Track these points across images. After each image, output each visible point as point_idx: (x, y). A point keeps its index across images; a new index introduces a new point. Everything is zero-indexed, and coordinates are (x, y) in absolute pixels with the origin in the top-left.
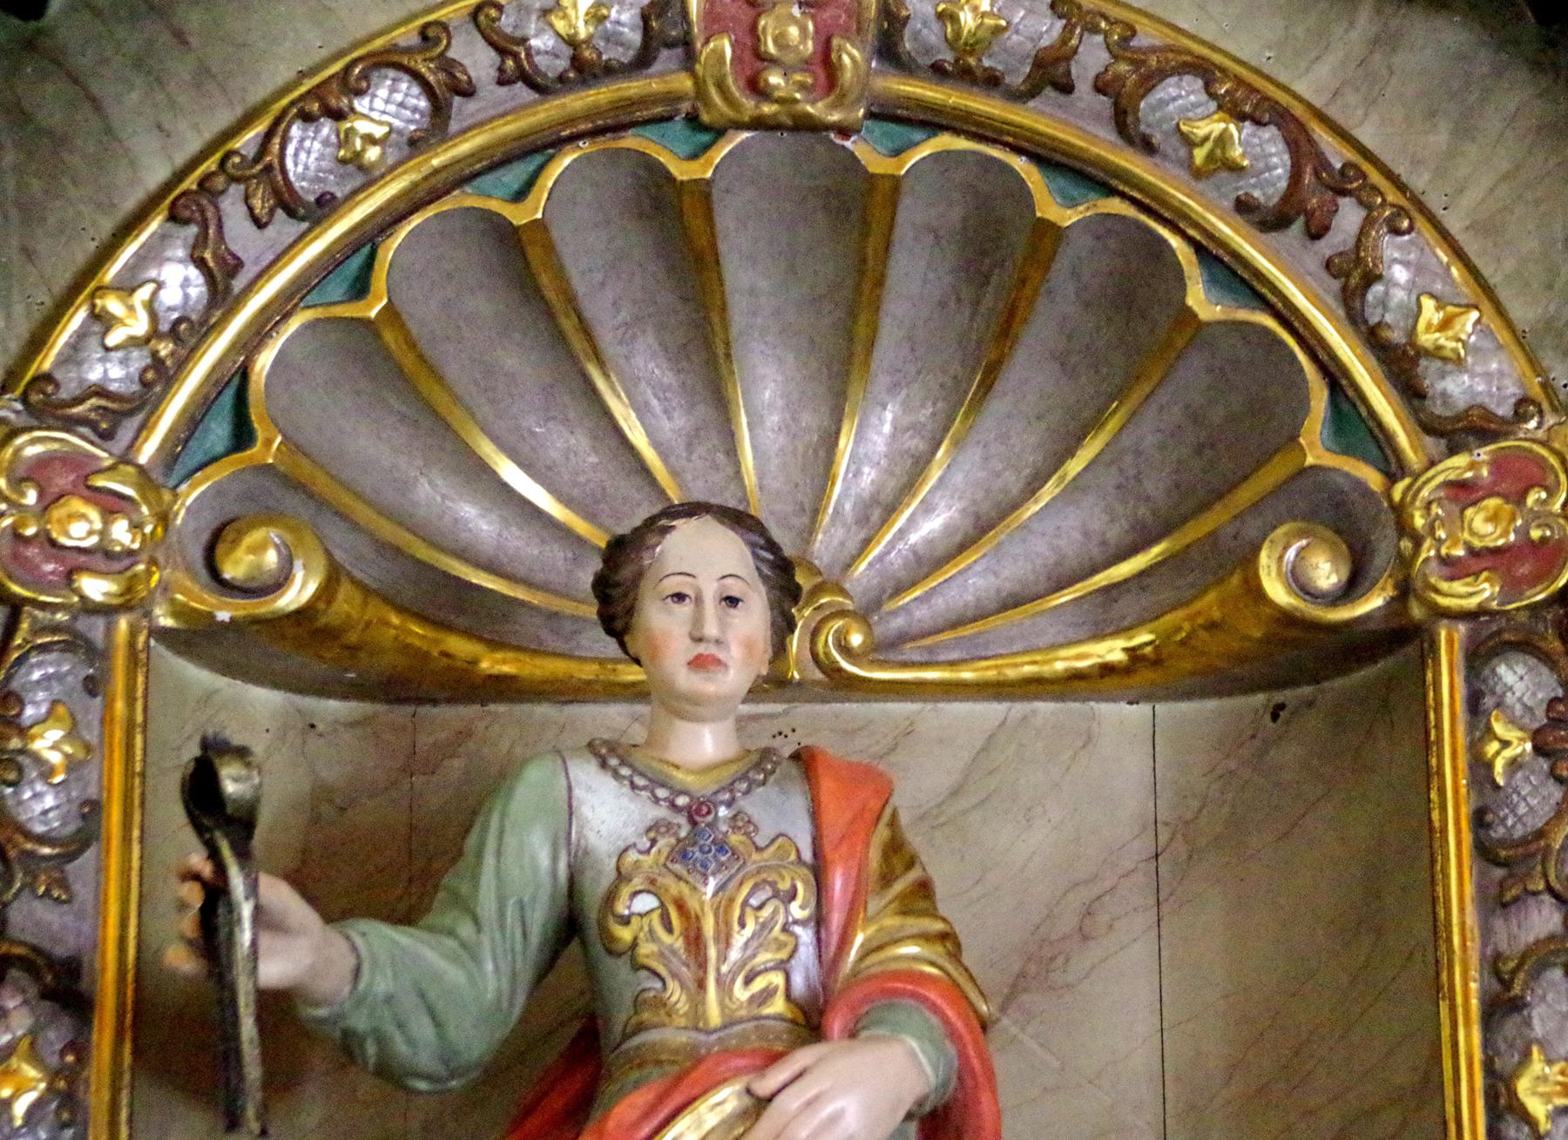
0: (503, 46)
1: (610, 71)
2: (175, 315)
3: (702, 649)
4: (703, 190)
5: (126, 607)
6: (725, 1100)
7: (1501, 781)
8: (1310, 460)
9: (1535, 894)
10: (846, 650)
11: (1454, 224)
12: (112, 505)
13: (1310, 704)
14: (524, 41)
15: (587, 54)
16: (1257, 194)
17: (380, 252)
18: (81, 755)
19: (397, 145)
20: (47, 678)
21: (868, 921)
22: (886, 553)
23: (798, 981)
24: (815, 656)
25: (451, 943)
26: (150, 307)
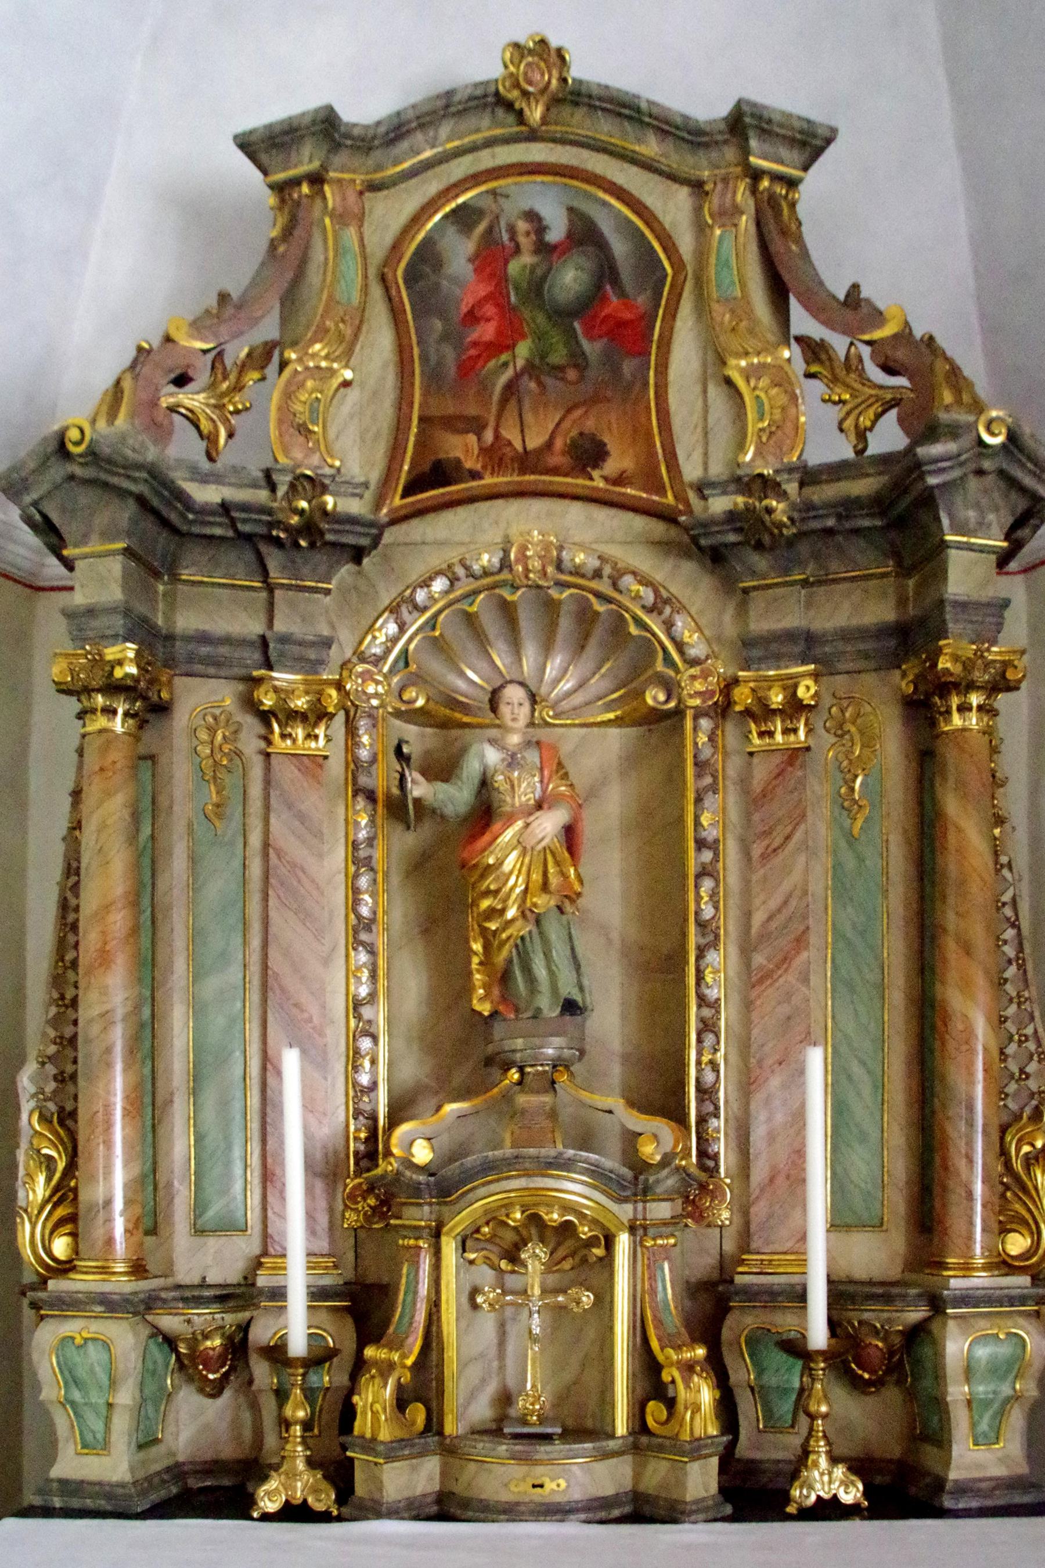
0: (467, 568)
1: (492, 574)
6: (520, 824)
11: (693, 613)
12: (377, 682)
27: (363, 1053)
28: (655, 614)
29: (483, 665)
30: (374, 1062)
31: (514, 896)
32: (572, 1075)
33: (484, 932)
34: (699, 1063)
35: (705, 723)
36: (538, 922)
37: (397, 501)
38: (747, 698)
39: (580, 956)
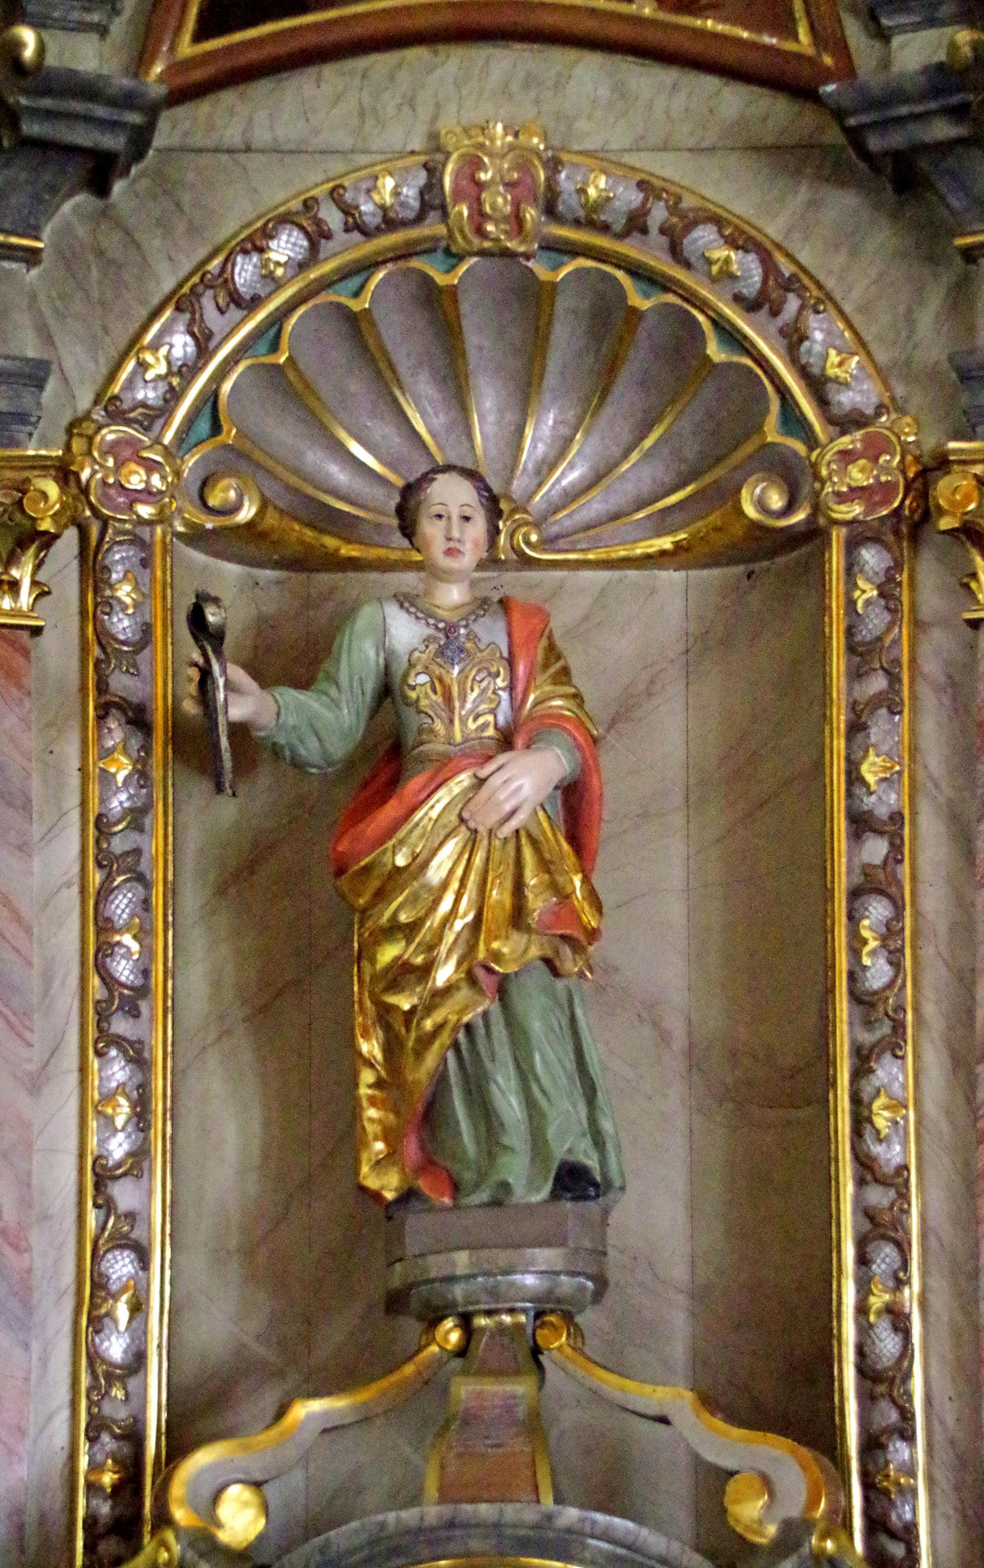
0: (347, 210)
1: (404, 224)
2: (180, 363)
3: (451, 544)
4: (453, 292)
5: (161, 522)
6: (464, 780)
7: (860, 611)
8: (769, 439)
9: (875, 670)
10: (528, 543)
11: (848, 308)
12: (150, 466)
13: (768, 570)
14: (357, 207)
15: (392, 214)
16: (745, 291)
17: (285, 326)
18: (141, 599)
19: (292, 267)
20: (122, 558)
21: (536, 688)
22: (550, 490)
23: (501, 720)
24: (513, 548)
25: (324, 698)
26: (168, 358)
27: (114, 1287)
28: (764, 313)
29: (385, 431)
30: (138, 1308)
31: (449, 937)
32: (576, 1332)
33: (385, 1013)
34: (862, 1310)
35: (871, 557)
36: (503, 990)
37: (186, 48)
38: (967, 499)
39: (595, 1069)
